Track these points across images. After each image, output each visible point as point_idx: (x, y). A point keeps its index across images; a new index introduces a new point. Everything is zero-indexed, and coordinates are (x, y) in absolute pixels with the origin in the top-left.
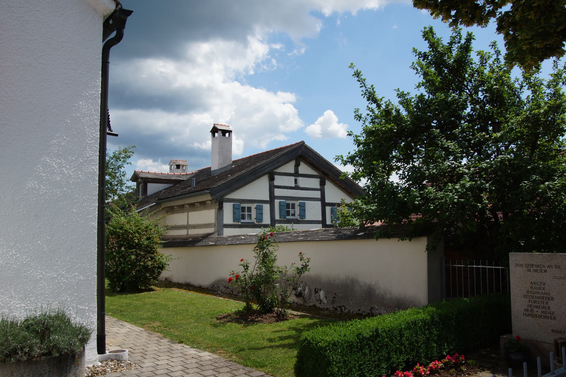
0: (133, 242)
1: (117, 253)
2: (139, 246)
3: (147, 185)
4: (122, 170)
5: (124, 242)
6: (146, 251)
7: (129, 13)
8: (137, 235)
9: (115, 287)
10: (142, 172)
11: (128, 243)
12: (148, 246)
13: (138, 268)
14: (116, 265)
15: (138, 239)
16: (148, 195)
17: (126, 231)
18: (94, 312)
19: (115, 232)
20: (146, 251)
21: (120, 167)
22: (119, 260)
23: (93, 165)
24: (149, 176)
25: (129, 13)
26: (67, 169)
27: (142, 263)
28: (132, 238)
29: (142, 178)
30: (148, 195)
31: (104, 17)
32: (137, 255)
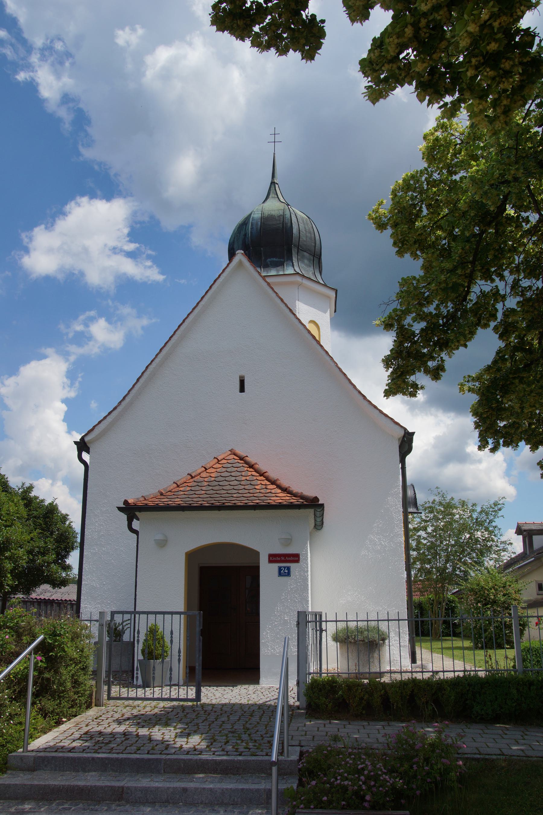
0: (490, 598)
1: (475, 609)
2: (494, 602)
3: (532, 537)
4: (494, 524)
5: (481, 598)
6: (503, 607)
7: (413, 433)
8: (493, 591)
9: (477, 644)
10: (526, 523)
11: (485, 599)
12: (505, 602)
13: (496, 624)
14: (476, 621)
15: (494, 596)
16: (535, 549)
17: (482, 587)
18: (406, 634)
19: (472, 589)
20: (503, 607)
21: (491, 521)
22: (478, 616)
23: (400, 537)
24: (533, 527)
25: (413, 433)
26: (384, 541)
27: (499, 619)
28: (488, 595)
29: (525, 531)
30: (535, 549)
31: (399, 439)
32: (494, 611)
